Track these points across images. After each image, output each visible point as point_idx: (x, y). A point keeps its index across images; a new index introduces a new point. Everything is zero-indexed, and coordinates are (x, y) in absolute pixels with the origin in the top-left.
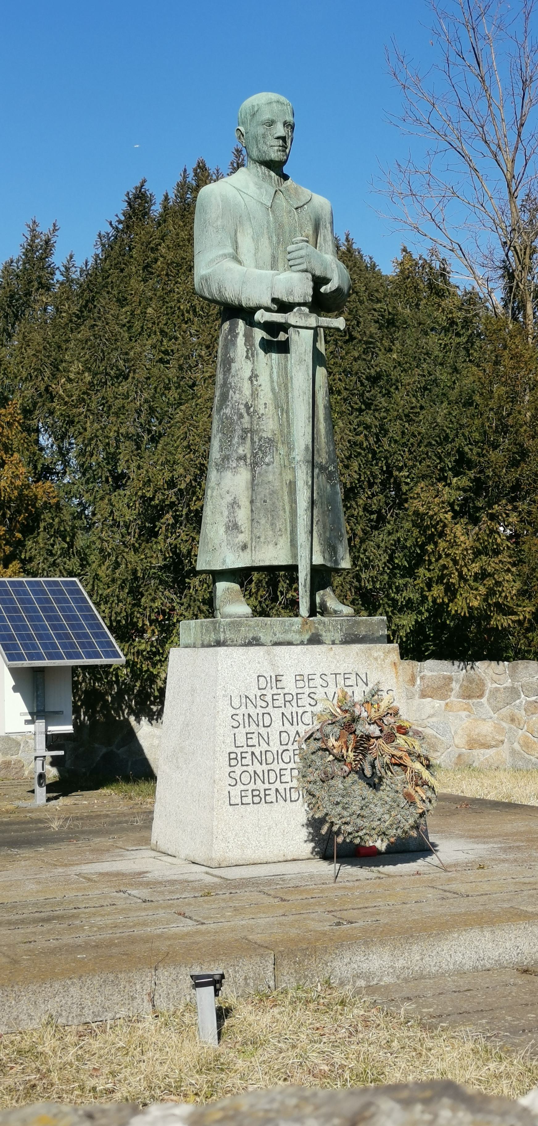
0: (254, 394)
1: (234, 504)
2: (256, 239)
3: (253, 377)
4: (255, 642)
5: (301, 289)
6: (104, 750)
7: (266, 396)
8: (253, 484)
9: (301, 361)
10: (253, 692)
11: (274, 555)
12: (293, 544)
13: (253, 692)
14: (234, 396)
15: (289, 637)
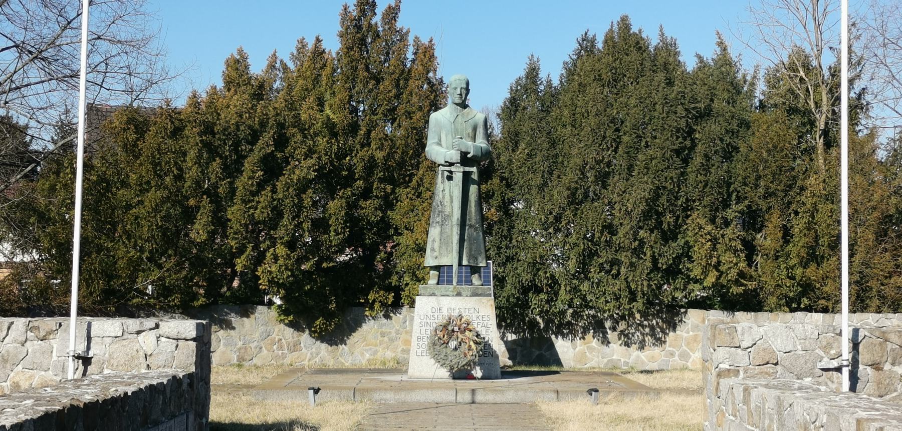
0: (443, 197)
1: (434, 240)
2: (446, 136)
4: (433, 295)
5: (455, 156)
6: (537, 353)
7: (447, 198)
8: (441, 233)
10: (430, 313)
11: (445, 261)
12: (450, 258)
13: (430, 313)
14: (437, 198)
15: (447, 293)
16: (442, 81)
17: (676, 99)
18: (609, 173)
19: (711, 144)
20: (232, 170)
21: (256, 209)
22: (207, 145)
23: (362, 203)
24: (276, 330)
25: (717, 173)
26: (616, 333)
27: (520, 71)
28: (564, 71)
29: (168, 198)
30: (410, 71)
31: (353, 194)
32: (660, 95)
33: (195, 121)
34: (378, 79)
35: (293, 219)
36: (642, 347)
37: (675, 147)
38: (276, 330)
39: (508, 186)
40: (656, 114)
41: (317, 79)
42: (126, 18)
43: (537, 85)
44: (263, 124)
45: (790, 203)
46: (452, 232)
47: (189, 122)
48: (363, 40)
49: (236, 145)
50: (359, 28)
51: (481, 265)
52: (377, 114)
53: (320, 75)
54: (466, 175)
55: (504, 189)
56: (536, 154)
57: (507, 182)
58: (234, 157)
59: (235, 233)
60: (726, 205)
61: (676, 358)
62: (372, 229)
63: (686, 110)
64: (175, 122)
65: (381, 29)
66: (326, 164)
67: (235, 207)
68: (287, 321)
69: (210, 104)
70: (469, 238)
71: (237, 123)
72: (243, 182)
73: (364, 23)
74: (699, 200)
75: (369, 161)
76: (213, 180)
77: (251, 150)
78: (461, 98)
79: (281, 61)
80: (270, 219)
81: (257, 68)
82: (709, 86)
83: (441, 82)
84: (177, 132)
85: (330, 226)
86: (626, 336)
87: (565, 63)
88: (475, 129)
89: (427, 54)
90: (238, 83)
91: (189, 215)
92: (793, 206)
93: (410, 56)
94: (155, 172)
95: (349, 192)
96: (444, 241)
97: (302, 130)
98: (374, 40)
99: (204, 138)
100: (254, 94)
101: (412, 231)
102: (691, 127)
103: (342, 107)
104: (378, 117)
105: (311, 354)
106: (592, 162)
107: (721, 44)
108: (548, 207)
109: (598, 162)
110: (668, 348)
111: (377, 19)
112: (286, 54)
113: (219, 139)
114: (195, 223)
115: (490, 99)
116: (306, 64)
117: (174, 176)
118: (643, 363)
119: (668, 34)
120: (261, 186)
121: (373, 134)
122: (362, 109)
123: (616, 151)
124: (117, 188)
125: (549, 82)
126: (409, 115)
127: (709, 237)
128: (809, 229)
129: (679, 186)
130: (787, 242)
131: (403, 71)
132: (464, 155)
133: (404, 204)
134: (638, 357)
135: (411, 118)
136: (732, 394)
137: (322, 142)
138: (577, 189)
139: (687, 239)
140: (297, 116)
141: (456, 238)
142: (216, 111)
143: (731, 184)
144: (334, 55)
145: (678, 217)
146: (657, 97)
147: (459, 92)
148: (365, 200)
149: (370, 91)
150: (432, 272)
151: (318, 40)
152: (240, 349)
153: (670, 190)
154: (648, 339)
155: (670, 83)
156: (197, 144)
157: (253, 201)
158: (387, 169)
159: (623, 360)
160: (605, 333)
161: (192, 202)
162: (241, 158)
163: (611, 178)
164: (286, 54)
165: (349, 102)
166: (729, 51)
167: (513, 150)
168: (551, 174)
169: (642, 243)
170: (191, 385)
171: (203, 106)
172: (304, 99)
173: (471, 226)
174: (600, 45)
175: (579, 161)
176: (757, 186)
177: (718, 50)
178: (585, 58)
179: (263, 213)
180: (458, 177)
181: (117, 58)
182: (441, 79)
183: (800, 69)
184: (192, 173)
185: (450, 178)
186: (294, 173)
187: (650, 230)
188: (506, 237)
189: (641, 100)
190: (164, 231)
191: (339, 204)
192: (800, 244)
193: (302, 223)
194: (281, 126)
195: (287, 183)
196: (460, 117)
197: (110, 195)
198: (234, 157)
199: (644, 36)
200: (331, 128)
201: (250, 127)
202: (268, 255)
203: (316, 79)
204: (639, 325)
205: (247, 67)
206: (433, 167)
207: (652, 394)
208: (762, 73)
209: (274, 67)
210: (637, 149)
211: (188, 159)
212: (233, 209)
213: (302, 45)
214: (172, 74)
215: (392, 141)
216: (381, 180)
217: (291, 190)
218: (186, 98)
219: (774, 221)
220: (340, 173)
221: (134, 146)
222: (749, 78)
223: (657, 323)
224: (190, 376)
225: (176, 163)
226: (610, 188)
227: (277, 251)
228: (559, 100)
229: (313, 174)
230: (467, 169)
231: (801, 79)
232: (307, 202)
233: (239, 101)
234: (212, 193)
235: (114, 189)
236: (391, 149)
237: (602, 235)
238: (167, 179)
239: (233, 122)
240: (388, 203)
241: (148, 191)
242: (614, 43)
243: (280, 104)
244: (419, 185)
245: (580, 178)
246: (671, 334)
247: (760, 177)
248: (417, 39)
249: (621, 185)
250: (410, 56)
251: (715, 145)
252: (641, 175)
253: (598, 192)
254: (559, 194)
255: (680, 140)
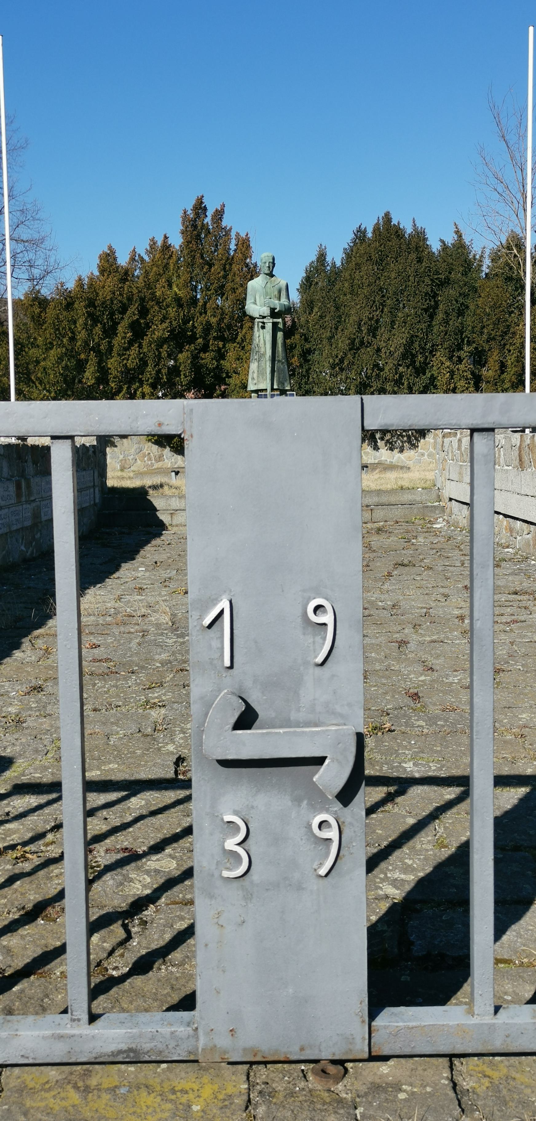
0: (259, 341)
1: (253, 372)
3: (259, 336)
5: (266, 311)
7: (262, 341)
8: (258, 367)
9: (268, 332)
11: (261, 386)
12: (265, 384)
14: (254, 342)
16: (256, 265)
17: (424, 272)
18: (378, 328)
19: (450, 304)
20: (110, 332)
21: (128, 360)
22: (90, 315)
23: (202, 355)
24: (146, 447)
25: (455, 323)
26: (384, 442)
27: (313, 257)
28: (344, 256)
29: (66, 354)
30: (233, 258)
31: (196, 349)
32: (412, 269)
33: (81, 297)
34: (211, 265)
35: (155, 366)
36: (402, 451)
37: (424, 307)
38: (146, 447)
39: (306, 340)
40: (410, 283)
41: (166, 266)
42: (26, 223)
43: (325, 266)
44: (130, 299)
45: (505, 345)
46: (266, 366)
47: (77, 298)
48: (198, 237)
49: (112, 314)
50: (195, 226)
51: (287, 388)
52: (210, 290)
53: (168, 264)
54: (275, 325)
55: (303, 342)
56: (326, 316)
57: (305, 337)
58: (110, 323)
59: (114, 378)
60: (460, 348)
61: (426, 457)
62: (210, 374)
63: (431, 280)
64: (68, 301)
65: (211, 227)
66: (176, 327)
67: (113, 359)
68: (153, 440)
69: (91, 286)
70: (278, 369)
71: (111, 298)
72: (117, 341)
73: (199, 223)
74: (441, 344)
75: (206, 325)
76: (96, 341)
77: (122, 318)
78: (269, 269)
79: (139, 255)
80: (138, 368)
81: (123, 260)
82: (448, 263)
83: (255, 265)
84: (69, 306)
85: (181, 371)
86: (391, 443)
87: (345, 249)
88: (280, 292)
89: (245, 245)
90: (110, 271)
91: (81, 366)
92: (507, 347)
93: (233, 247)
94: (56, 335)
95: (192, 347)
96: (261, 372)
97: (158, 303)
98: (206, 236)
99: (89, 310)
100: (121, 279)
101: (239, 374)
102: (435, 293)
103: (185, 286)
104: (211, 292)
105: (171, 463)
106: (365, 319)
107: (457, 232)
108: (334, 353)
109: (371, 319)
110: (420, 451)
111: (208, 220)
112: (142, 251)
113: (99, 311)
114: (85, 372)
115: (291, 275)
116: (157, 256)
117: (69, 337)
118: (402, 461)
119: (419, 225)
120: (131, 343)
121: (208, 305)
122: (200, 287)
123: (382, 311)
124: (29, 348)
125: (334, 264)
126: (234, 290)
127: (448, 370)
128: (518, 361)
129: (427, 335)
130: (503, 372)
131: (228, 259)
132: (272, 310)
133: (231, 355)
134: (399, 457)
135: (235, 293)
136: (452, 445)
137: (172, 312)
138: (355, 339)
139: (433, 372)
140: (153, 294)
141: (269, 370)
142: (95, 291)
143: (464, 332)
144: (178, 248)
145: (427, 357)
146: (410, 271)
147: (267, 265)
148: (205, 353)
149: (205, 274)
150: (253, 395)
151: (166, 237)
152: (121, 460)
153: (421, 338)
154: (406, 445)
155: (420, 260)
156: (84, 314)
157: (126, 354)
158: (220, 330)
159: (388, 460)
160: (376, 442)
161: (83, 356)
162: (116, 324)
163: (379, 330)
164: (142, 251)
165: (190, 282)
166: (463, 237)
167: (310, 313)
168: (337, 329)
169: (401, 376)
170: (94, 452)
171: (86, 287)
172: (158, 281)
173: (279, 361)
174: (370, 235)
175: (356, 319)
176: (482, 333)
177: (456, 237)
178: (359, 244)
179: (133, 362)
180: (269, 326)
181: (21, 255)
182: (256, 263)
183: (514, 248)
184: (82, 335)
185: (263, 327)
186: (155, 334)
187: (407, 366)
188: (305, 376)
189: (399, 274)
190: (65, 377)
191: (186, 356)
192: (512, 373)
193: (161, 369)
194: (142, 300)
195: (150, 341)
196: (269, 283)
197: (24, 353)
198: (110, 323)
199: (401, 227)
200: (178, 301)
201: (121, 302)
202: (138, 393)
203: (165, 266)
204: (399, 435)
205: (115, 259)
206: (252, 319)
207: (405, 469)
208: (487, 252)
209: (134, 259)
210: (397, 309)
211: (78, 325)
212: (111, 361)
213: (153, 243)
214: (61, 265)
215: (222, 309)
216: (215, 338)
217: (153, 346)
218: (74, 282)
219: (494, 358)
220: (186, 333)
221: (39, 317)
222: (477, 257)
223: (412, 434)
224: (93, 446)
225: (70, 329)
226: (378, 337)
227: (144, 390)
228: (341, 276)
229: (167, 334)
230: (275, 320)
231: (515, 256)
232: (164, 354)
233: (111, 282)
234: (96, 349)
235: (27, 349)
236: (221, 315)
237: (373, 371)
238: (65, 340)
239: (108, 298)
240: (221, 355)
241: (51, 349)
242: (380, 232)
243: (141, 283)
244: (243, 341)
245: (357, 331)
246: (422, 440)
247: (484, 327)
248: (238, 235)
249: (386, 336)
250: (233, 247)
251: (452, 304)
252: (400, 327)
253: (370, 341)
254: (342, 343)
255: (428, 301)
